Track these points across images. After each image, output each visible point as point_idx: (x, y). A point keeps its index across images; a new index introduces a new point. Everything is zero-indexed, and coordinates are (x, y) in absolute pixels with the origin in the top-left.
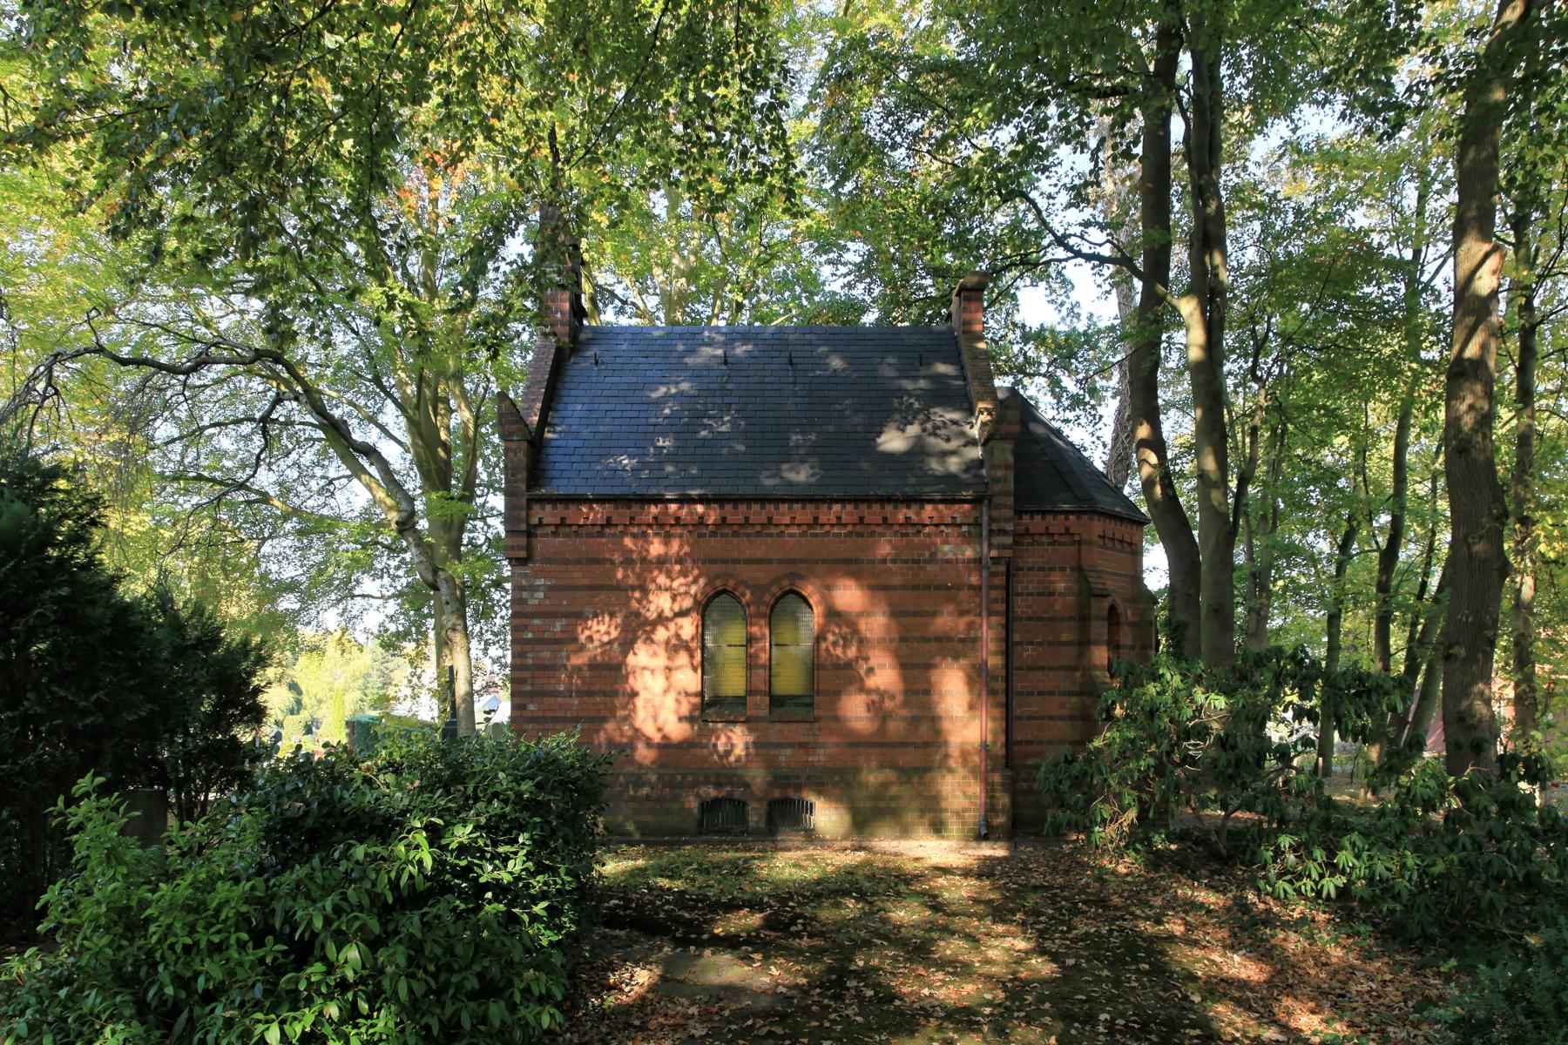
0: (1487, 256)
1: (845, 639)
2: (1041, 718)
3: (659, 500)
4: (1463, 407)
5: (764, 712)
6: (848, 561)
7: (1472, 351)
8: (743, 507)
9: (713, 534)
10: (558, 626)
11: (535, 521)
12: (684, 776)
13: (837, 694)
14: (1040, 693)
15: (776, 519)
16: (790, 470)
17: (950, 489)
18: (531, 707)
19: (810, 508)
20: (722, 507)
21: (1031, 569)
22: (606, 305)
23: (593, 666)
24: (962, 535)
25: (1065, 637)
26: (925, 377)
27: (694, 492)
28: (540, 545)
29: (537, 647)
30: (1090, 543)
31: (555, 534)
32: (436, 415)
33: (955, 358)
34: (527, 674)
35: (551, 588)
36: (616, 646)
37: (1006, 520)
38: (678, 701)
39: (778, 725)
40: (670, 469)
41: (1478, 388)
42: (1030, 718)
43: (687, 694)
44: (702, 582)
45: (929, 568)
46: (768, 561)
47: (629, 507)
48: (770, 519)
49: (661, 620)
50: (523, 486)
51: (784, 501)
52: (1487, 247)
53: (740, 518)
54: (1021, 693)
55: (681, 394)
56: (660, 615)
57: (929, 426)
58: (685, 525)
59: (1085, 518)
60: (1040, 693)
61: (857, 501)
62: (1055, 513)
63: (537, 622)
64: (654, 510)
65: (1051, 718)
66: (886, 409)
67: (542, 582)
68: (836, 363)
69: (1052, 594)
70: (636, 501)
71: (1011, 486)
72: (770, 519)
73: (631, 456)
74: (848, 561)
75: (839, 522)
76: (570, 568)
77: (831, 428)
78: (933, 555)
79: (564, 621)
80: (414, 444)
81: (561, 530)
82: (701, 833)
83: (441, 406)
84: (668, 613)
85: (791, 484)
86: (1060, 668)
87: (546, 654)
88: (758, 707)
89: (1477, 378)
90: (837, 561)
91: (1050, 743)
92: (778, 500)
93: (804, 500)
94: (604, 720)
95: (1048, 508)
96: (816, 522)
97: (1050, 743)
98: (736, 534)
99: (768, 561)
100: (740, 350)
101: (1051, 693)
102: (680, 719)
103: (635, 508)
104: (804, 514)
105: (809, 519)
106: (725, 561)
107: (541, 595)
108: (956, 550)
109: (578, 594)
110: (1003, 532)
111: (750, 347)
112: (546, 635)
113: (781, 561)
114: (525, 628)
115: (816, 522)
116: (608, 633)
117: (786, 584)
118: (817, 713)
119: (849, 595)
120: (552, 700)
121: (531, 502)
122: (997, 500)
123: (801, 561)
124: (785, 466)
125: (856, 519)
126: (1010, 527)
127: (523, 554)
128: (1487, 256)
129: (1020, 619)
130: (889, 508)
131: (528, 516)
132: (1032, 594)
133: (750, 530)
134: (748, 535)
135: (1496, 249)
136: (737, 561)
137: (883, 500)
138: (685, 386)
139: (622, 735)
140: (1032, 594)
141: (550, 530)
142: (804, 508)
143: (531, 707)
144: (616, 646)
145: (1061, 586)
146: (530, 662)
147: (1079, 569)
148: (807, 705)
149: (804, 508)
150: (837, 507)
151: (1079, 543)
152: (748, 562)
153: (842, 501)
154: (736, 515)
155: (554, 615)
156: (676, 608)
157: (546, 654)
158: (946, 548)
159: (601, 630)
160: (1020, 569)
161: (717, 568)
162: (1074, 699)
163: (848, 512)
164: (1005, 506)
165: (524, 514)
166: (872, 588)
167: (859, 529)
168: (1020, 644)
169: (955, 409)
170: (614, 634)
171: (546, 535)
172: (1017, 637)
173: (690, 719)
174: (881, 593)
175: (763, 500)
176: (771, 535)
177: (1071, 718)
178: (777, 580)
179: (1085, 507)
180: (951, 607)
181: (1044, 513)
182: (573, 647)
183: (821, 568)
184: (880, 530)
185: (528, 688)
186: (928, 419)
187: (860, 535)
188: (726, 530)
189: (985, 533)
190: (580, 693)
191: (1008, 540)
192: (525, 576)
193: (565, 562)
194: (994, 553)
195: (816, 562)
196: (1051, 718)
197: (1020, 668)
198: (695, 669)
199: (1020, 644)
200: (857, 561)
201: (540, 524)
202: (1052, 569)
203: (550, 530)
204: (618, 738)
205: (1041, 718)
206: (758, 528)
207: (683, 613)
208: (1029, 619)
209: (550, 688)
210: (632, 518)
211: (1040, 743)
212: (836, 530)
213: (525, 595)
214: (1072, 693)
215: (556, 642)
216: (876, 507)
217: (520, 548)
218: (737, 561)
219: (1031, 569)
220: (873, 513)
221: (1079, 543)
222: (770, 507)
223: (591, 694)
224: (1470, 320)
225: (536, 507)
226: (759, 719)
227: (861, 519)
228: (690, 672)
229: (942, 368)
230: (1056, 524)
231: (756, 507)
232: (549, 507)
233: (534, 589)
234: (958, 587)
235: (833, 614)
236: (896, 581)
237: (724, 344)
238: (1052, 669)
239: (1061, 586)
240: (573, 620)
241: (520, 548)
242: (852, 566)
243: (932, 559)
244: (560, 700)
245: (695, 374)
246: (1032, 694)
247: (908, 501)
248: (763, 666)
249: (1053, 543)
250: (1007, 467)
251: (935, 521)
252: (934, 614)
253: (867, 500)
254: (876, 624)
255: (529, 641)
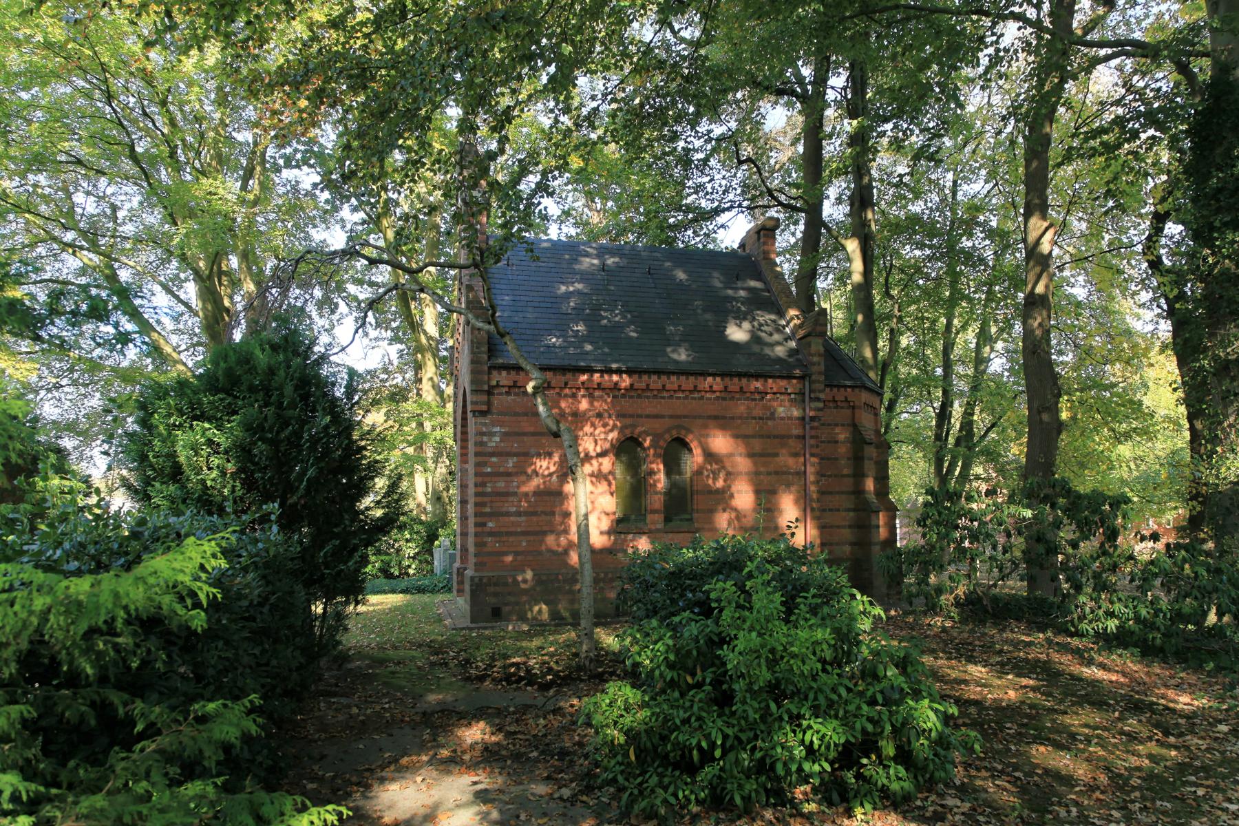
0: (1047, 229)
1: (714, 473)
2: (831, 527)
3: (590, 370)
4: (1036, 324)
5: (660, 526)
6: (716, 418)
7: (1040, 289)
8: (645, 377)
9: (623, 396)
10: (511, 463)
11: (494, 383)
12: (606, 574)
13: (712, 511)
14: (831, 510)
15: (668, 386)
16: (673, 351)
17: (781, 370)
18: (490, 525)
19: (692, 379)
22: (342, 204)
23: (538, 493)
24: (791, 400)
25: (846, 471)
26: (743, 289)
27: (614, 366)
28: (496, 401)
29: (494, 479)
30: (860, 408)
31: (508, 393)
32: (221, 284)
33: (758, 277)
34: (486, 499)
35: (505, 434)
36: (554, 478)
37: (820, 391)
38: (599, 519)
39: (670, 535)
40: (589, 347)
41: (1045, 313)
43: (607, 514)
45: (770, 423)
46: (662, 417)
47: (564, 375)
48: (664, 386)
49: (588, 458)
50: (485, 357)
51: (674, 373)
52: (1046, 224)
53: (643, 385)
55: (578, 292)
56: (587, 455)
57: (756, 324)
58: (604, 389)
59: (857, 390)
60: (831, 510)
61: (723, 375)
62: (839, 387)
63: (494, 459)
64: (585, 377)
65: (838, 527)
66: (724, 311)
67: (498, 429)
68: (681, 275)
69: (837, 442)
70: (569, 370)
71: (822, 368)
72: (664, 386)
73: (558, 338)
75: (711, 391)
76: (520, 419)
77: (691, 322)
78: (773, 414)
79: (515, 459)
80: (204, 309)
81: (512, 390)
82: (618, 616)
83: (224, 278)
84: (593, 454)
85: (676, 362)
86: (842, 493)
87: (501, 484)
88: (653, 523)
89: (1044, 307)
90: (709, 417)
92: (669, 373)
93: (687, 373)
94: (544, 533)
96: (695, 389)
98: (639, 396)
99: (662, 417)
100: (611, 261)
101: (838, 510)
102: (602, 533)
103: (569, 376)
104: (688, 383)
105: (691, 387)
106: (632, 416)
107: (497, 439)
108: (787, 410)
109: (525, 439)
110: (818, 399)
111: (617, 260)
112: (502, 470)
113: (671, 417)
114: (485, 464)
115: (695, 389)
116: (548, 468)
117: (675, 434)
118: (696, 525)
119: (721, 442)
120: (506, 519)
122: (813, 377)
123: (685, 417)
124: (669, 349)
125: (721, 387)
126: (822, 396)
127: (484, 408)
128: (1047, 229)
130: (744, 381)
131: (489, 379)
133: (649, 394)
134: (648, 397)
135: (1051, 226)
136: (640, 416)
137: (740, 375)
138: (579, 286)
139: (559, 545)
141: (504, 390)
143: (490, 525)
144: (554, 478)
145: (842, 437)
146: (489, 490)
147: (854, 426)
148: (688, 520)
150: (710, 379)
151: (853, 407)
152: (648, 416)
153: (714, 375)
155: (509, 454)
156: (599, 450)
157: (501, 484)
158: (781, 409)
159: (546, 466)
161: (628, 421)
162: (852, 514)
163: (717, 383)
164: (819, 382)
165: (486, 377)
166: (736, 437)
167: (723, 395)
169: (770, 312)
170: (553, 469)
171: (500, 394)
173: (609, 533)
174: (739, 441)
175: (659, 373)
176: (663, 398)
177: (850, 527)
178: (668, 431)
179: (859, 383)
180: (784, 451)
182: (523, 478)
183: (699, 422)
184: (738, 396)
185: (488, 510)
186: (754, 319)
187: (724, 399)
188: (633, 393)
189: (807, 399)
190: (526, 514)
191: (821, 405)
192: (485, 424)
193: (516, 414)
194: (812, 414)
195: (695, 417)
196: (838, 527)
198: (612, 494)
200: (724, 418)
201: (498, 386)
202: (837, 425)
203: (504, 390)
204: (555, 548)
205: (831, 527)
207: (603, 454)
209: (504, 509)
210: (566, 384)
212: (708, 395)
213: (485, 439)
214: (849, 510)
215: (508, 474)
216: (736, 380)
217: (482, 403)
218: (640, 416)
220: (734, 384)
221: (853, 407)
222: (664, 378)
223: (534, 514)
224: (1038, 269)
225: (495, 373)
226: (658, 530)
227: (726, 388)
228: (609, 497)
229: (753, 284)
231: (654, 377)
232: (504, 373)
233: (492, 434)
234: (789, 437)
235: (710, 456)
237: (598, 256)
238: (838, 493)
239: (842, 437)
240: (522, 458)
241: (482, 403)
242: (723, 422)
243: (772, 416)
244: (512, 518)
245: (585, 277)
247: (757, 376)
249: (837, 407)
250: (820, 355)
251: (775, 390)
252: (776, 455)
253: (730, 375)
254: (742, 463)
255: (488, 474)
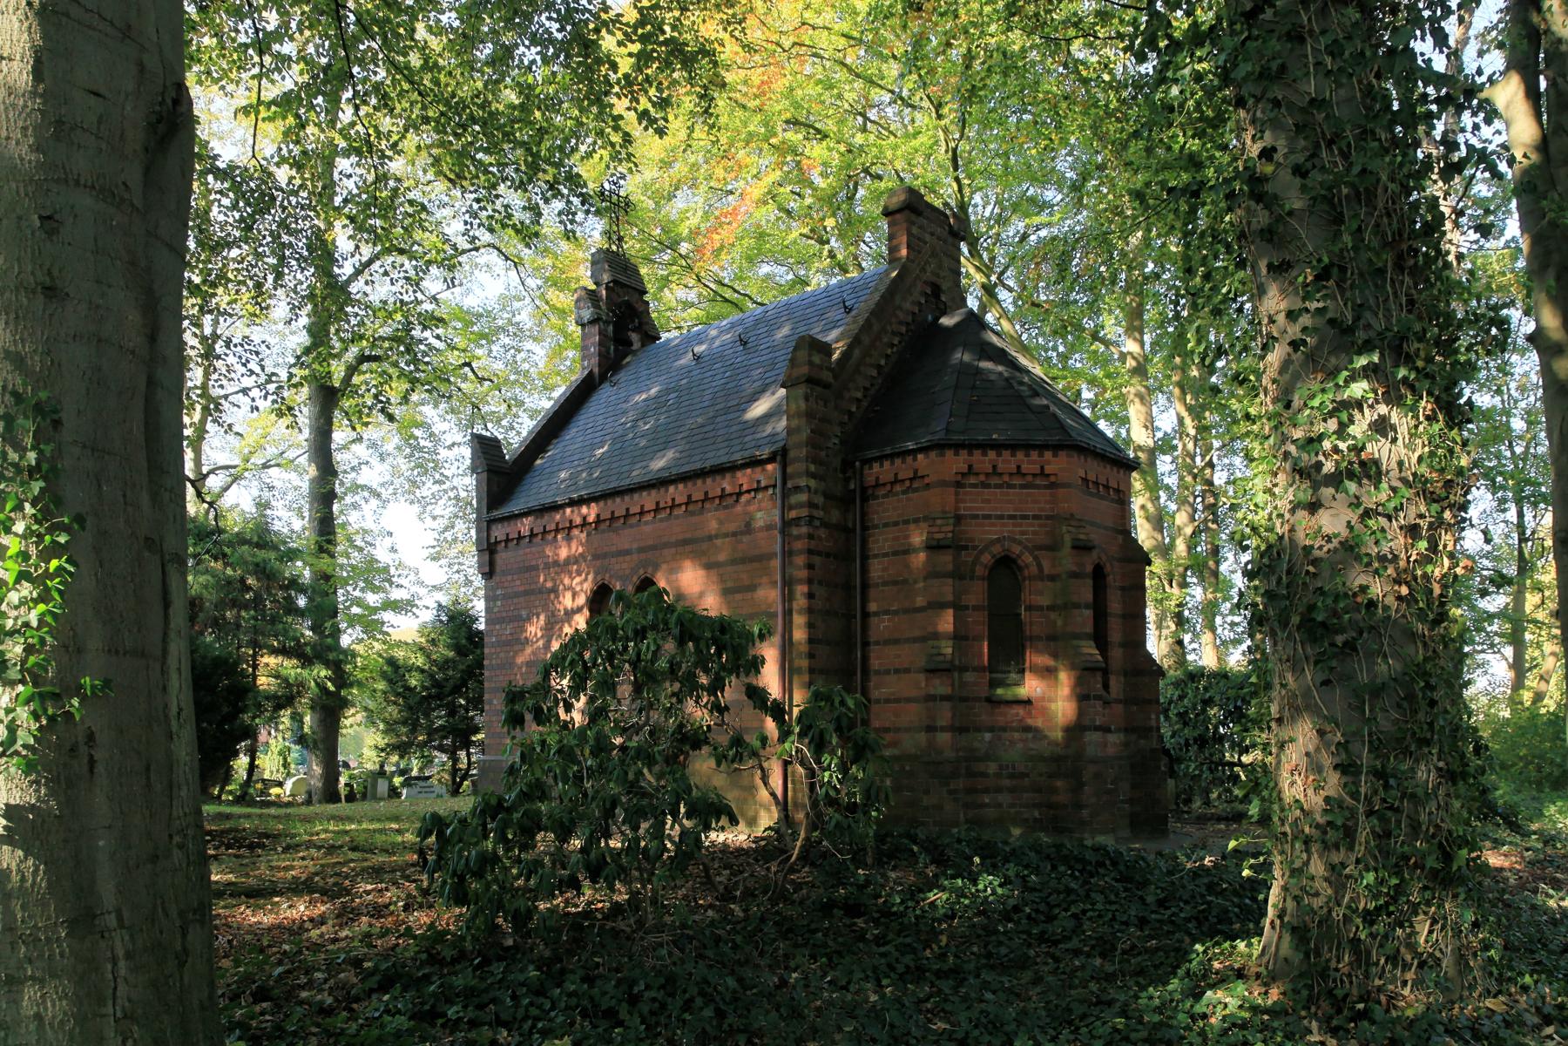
2: (898, 701)
6: (685, 542)
14: (897, 671)
20: (971, 454)
21: (886, 525)
42: (887, 701)
44: (590, 577)
53: (1036, 469)
54: (878, 673)
60: (897, 671)
74: (685, 542)
91: (908, 730)
95: (888, 451)
97: (908, 730)
101: (907, 671)
121: (490, 522)
129: (877, 585)
132: (886, 555)
140: (886, 555)
142: (957, 454)
149: (957, 454)
154: (618, 506)
160: (876, 527)
168: (876, 614)
172: (873, 607)
174: (714, 572)
181: (892, 456)
183: (667, 552)
197: (877, 643)
199: (876, 614)
205: (898, 701)
206: (982, 478)
208: (885, 583)
211: (898, 730)
219: (886, 525)
230: (903, 468)
236: (722, 557)
238: (908, 640)
246: (888, 672)
248: (799, 671)
